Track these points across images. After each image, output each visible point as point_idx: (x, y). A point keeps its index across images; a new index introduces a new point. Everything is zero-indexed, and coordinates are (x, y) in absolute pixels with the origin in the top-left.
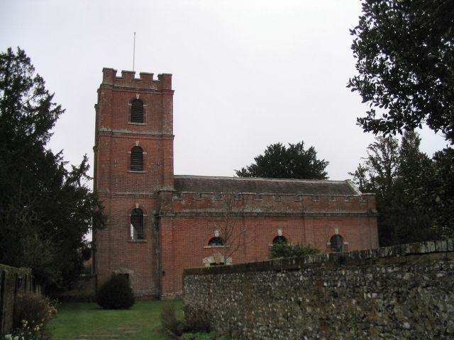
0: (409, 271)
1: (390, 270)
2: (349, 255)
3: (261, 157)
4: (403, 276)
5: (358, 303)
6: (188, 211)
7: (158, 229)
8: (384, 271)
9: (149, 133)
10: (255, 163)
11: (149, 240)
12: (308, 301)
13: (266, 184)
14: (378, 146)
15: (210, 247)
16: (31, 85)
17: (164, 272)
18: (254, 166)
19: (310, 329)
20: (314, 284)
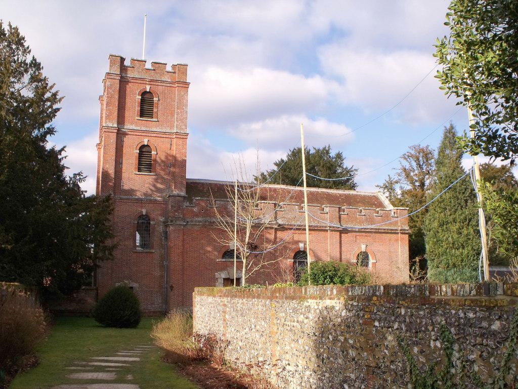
0: (500, 318)
1: (471, 315)
2: (413, 289)
3: (282, 161)
4: (490, 325)
5: (422, 352)
6: (200, 219)
7: (166, 238)
8: (462, 315)
9: (160, 130)
10: (275, 168)
11: (156, 251)
12: (351, 342)
13: (328, 195)
14: (412, 156)
15: (224, 260)
16: (26, 71)
17: (172, 288)
18: (273, 172)
19: (353, 376)
20: (361, 322)
